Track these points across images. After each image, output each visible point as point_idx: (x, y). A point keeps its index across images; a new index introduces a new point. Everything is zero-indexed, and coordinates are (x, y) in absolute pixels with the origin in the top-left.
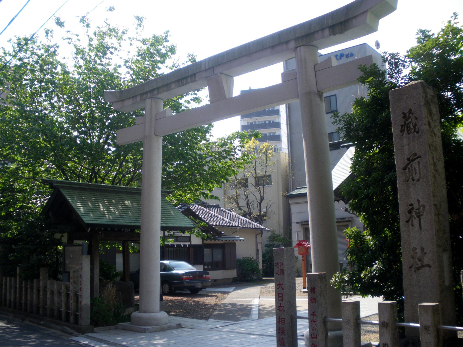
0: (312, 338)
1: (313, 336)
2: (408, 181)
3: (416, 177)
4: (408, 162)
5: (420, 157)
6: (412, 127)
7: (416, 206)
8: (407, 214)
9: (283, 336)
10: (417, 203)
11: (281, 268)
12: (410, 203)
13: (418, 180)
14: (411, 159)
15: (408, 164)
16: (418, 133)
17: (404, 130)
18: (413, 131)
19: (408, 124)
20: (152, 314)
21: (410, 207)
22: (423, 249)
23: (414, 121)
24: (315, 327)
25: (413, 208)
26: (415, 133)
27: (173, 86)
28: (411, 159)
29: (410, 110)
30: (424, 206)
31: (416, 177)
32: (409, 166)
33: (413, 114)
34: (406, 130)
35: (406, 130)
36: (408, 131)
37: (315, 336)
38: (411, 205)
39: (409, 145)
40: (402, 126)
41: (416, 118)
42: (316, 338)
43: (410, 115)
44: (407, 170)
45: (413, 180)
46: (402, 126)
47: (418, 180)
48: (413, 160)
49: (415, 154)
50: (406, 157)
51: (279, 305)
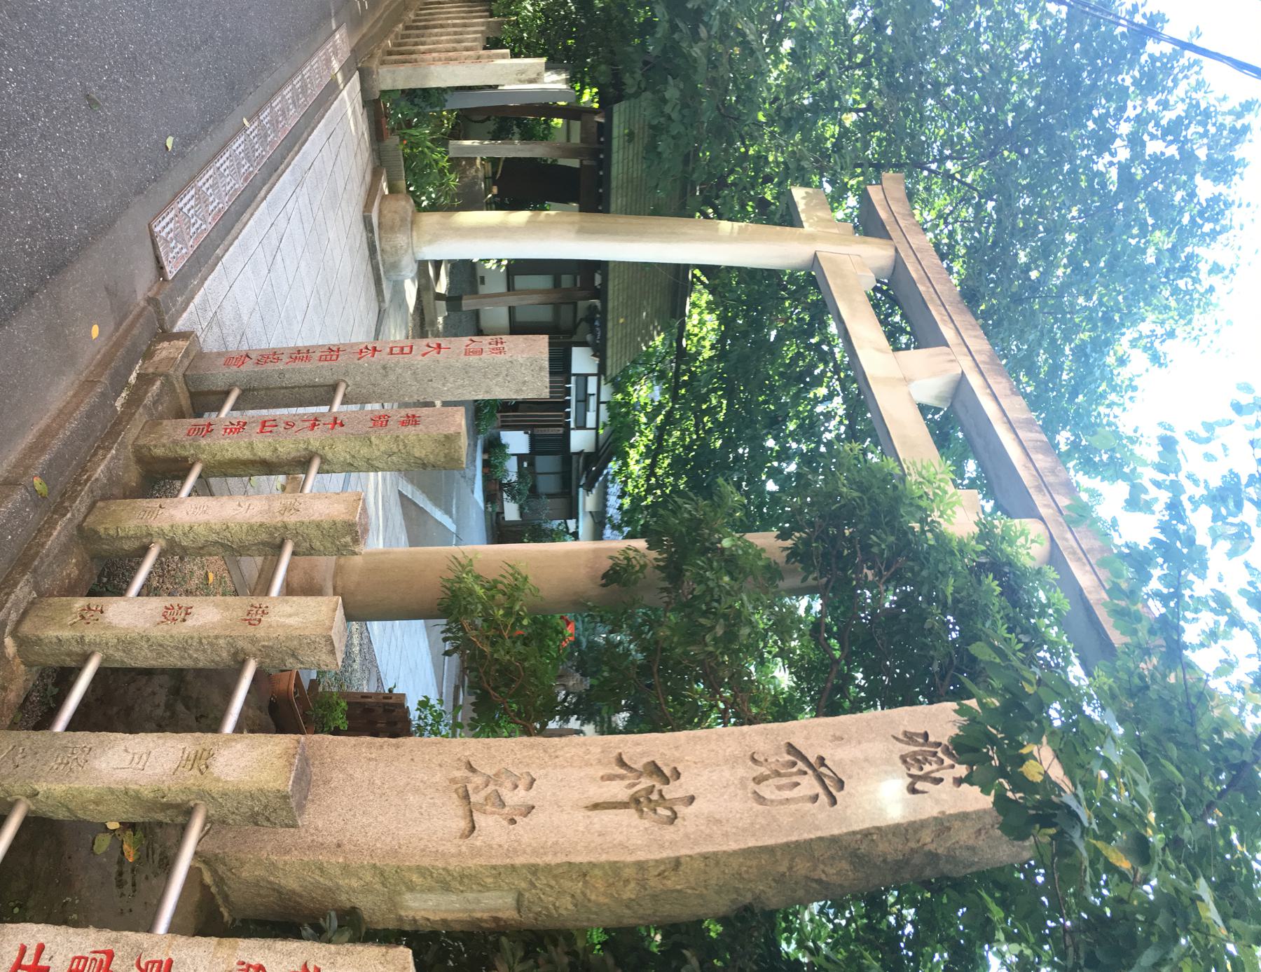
3: (767, 790)
4: (812, 760)
7: (673, 791)
10: (680, 794)
13: (760, 799)
15: (804, 759)
18: (915, 771)
21: (667, 771)
31: (767, 790)
32: (801, 765)
38: (677, 775)
45: (758, 780)
46: (926, 736)
47: (760, 799)
48: (820, 778)
49: (841, 784)
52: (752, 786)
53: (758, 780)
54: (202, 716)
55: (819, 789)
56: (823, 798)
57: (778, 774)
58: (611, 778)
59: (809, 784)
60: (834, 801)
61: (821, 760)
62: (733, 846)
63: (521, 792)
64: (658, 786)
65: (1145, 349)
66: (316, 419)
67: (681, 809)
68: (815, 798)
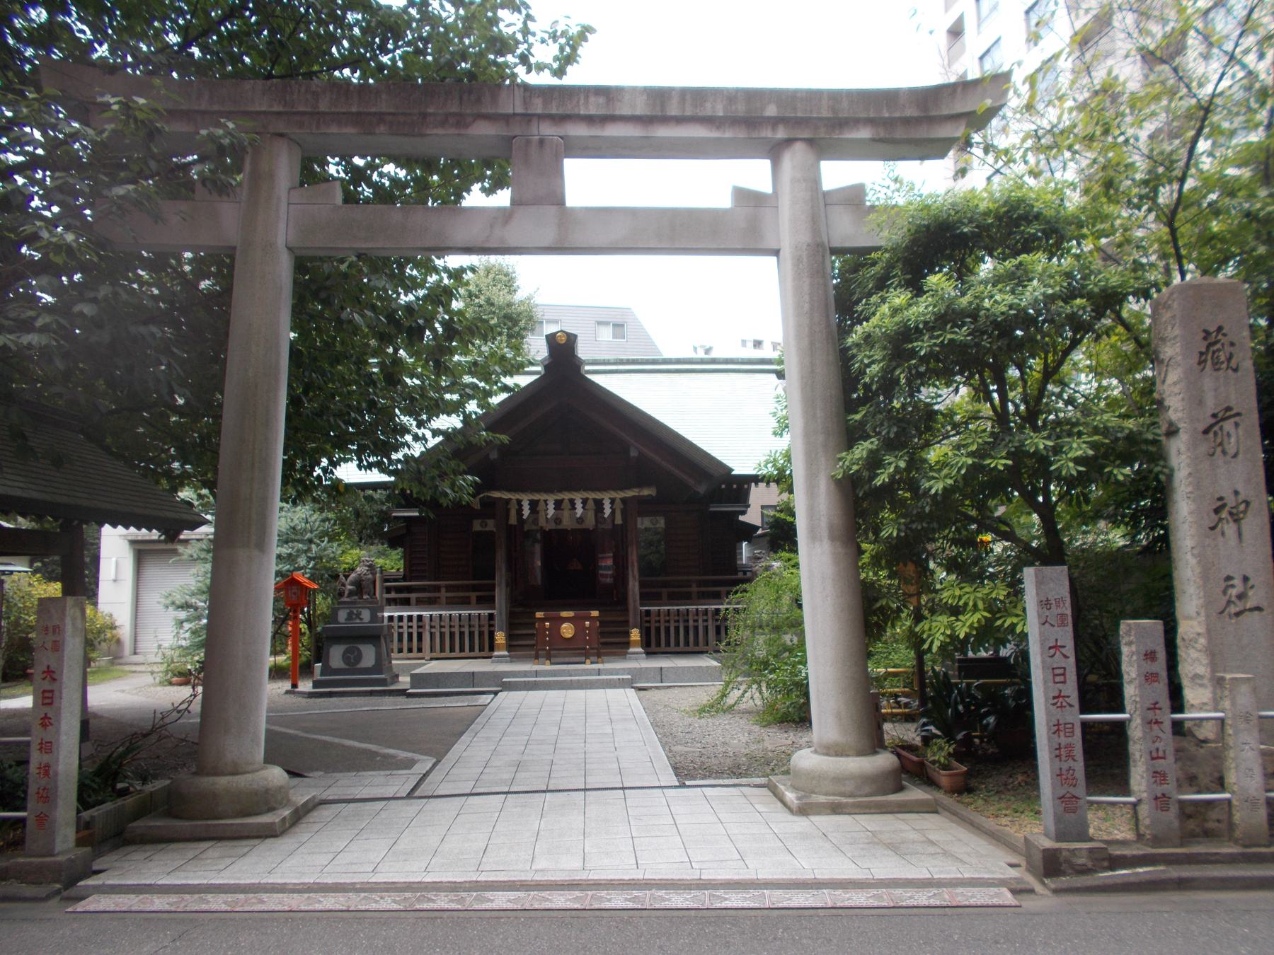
0: (1153, 759)
1: (1154, 755)
2: (1212, 455)
3: (1232, 451)
4: (1213, 421)
5: (1238, 414)
6: (1223, 358)
7: (1231, 501)
8: (1212, 514)
9: (1071, 763)
10: (1232, 497)
11: (1059, 611)
12: (1217, 496)
13: (1235, 456)
14: (1220, 415)
15: (1212, 426)
16: (1236, 370)
17: (1205, 361)
18: (1224, 366)
19: (1214, 352)
20: (249, 776)
21: (1219, 503)
22: (1246, 579)
23: (1228, 349)
24: (1161, 735)
25: (1224, 506)
26: (1230, 371)
27: (1239, 132)
28: (1220, 415)
29: (1220, 329)
30: (1247, 503)
31: (1231, 449)
32: (1216, 428)
33: (1225, 335)
34: (1209, 362)
35: (1209, 362)
36: (1214, 364)
37: (1161, 754)
38: (1221, 499)
39: (1216, 390)
40: (1201, 354)
41: (1232, 344)
42: (1164, 758)
43: (1220, 337)
44: (1211, 435)
45: (1224, 452)
46: (1201, 354)
47: (1235, 456)
48: (1224, 419)
49: (1228, 409)
50: (1210, 412)
51: (1056, 694)
52: (1228, 458)
53: (1224, 452)
54: (1157, 722)
55: (1232, 420)
56: (1237, 419)
57: (1221, 444)
58: (1223, 534)
59: (1228, 426)
60: (1238, 414)
61: (1214, 416)
62: (90, 899)
63: (1235, 582)
64: (1227, 508)
65: (933, 611)
66: (1150, 723)
67: (1241, 498)
68: (1237, 425)
